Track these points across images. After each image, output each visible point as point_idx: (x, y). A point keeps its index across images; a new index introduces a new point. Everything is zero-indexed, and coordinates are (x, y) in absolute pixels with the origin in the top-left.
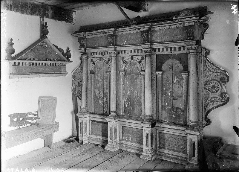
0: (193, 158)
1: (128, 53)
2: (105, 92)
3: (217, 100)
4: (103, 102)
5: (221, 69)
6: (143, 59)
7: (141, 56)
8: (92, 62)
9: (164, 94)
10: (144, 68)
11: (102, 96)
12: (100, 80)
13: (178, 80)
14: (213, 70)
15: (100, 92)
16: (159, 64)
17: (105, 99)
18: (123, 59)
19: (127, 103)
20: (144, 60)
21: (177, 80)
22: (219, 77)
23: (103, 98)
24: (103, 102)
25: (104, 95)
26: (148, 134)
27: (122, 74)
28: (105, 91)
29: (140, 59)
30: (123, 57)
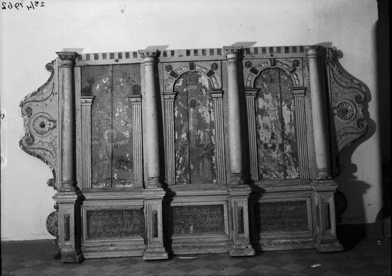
0: (241, 235)
1: (181, 56)
2: (286, 133)
3: (351, 131)
4: (284, 155)
5: (355, 81)
6: (217, 67)
7: (212, 63)
8: (250, 69)
9: (96, 139)
10: (218, 86)
11: (280, 141)
12: (272, 109)
13: (123, 112)
14: (343, 84)
15: (273, 134)
16: (87, 84)
17: (288, 148)
18: (169, 68)
19: (181, 158)
20: (219, 70)
21: (121, 111)
22: (354, 95)
23: (282, 146)
24: (284, 155)
25: (283, 139)
26: (242, 210)
27: (170, 98)
28: (288, 130)
29: (209, 68)
30: (168, 64)
